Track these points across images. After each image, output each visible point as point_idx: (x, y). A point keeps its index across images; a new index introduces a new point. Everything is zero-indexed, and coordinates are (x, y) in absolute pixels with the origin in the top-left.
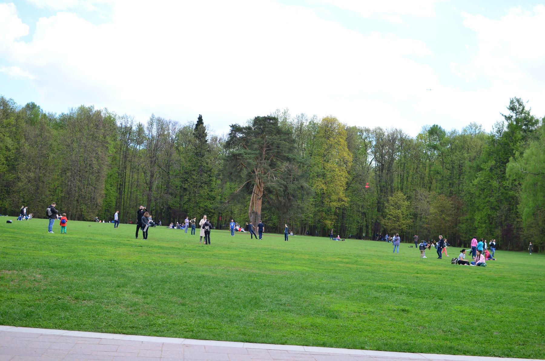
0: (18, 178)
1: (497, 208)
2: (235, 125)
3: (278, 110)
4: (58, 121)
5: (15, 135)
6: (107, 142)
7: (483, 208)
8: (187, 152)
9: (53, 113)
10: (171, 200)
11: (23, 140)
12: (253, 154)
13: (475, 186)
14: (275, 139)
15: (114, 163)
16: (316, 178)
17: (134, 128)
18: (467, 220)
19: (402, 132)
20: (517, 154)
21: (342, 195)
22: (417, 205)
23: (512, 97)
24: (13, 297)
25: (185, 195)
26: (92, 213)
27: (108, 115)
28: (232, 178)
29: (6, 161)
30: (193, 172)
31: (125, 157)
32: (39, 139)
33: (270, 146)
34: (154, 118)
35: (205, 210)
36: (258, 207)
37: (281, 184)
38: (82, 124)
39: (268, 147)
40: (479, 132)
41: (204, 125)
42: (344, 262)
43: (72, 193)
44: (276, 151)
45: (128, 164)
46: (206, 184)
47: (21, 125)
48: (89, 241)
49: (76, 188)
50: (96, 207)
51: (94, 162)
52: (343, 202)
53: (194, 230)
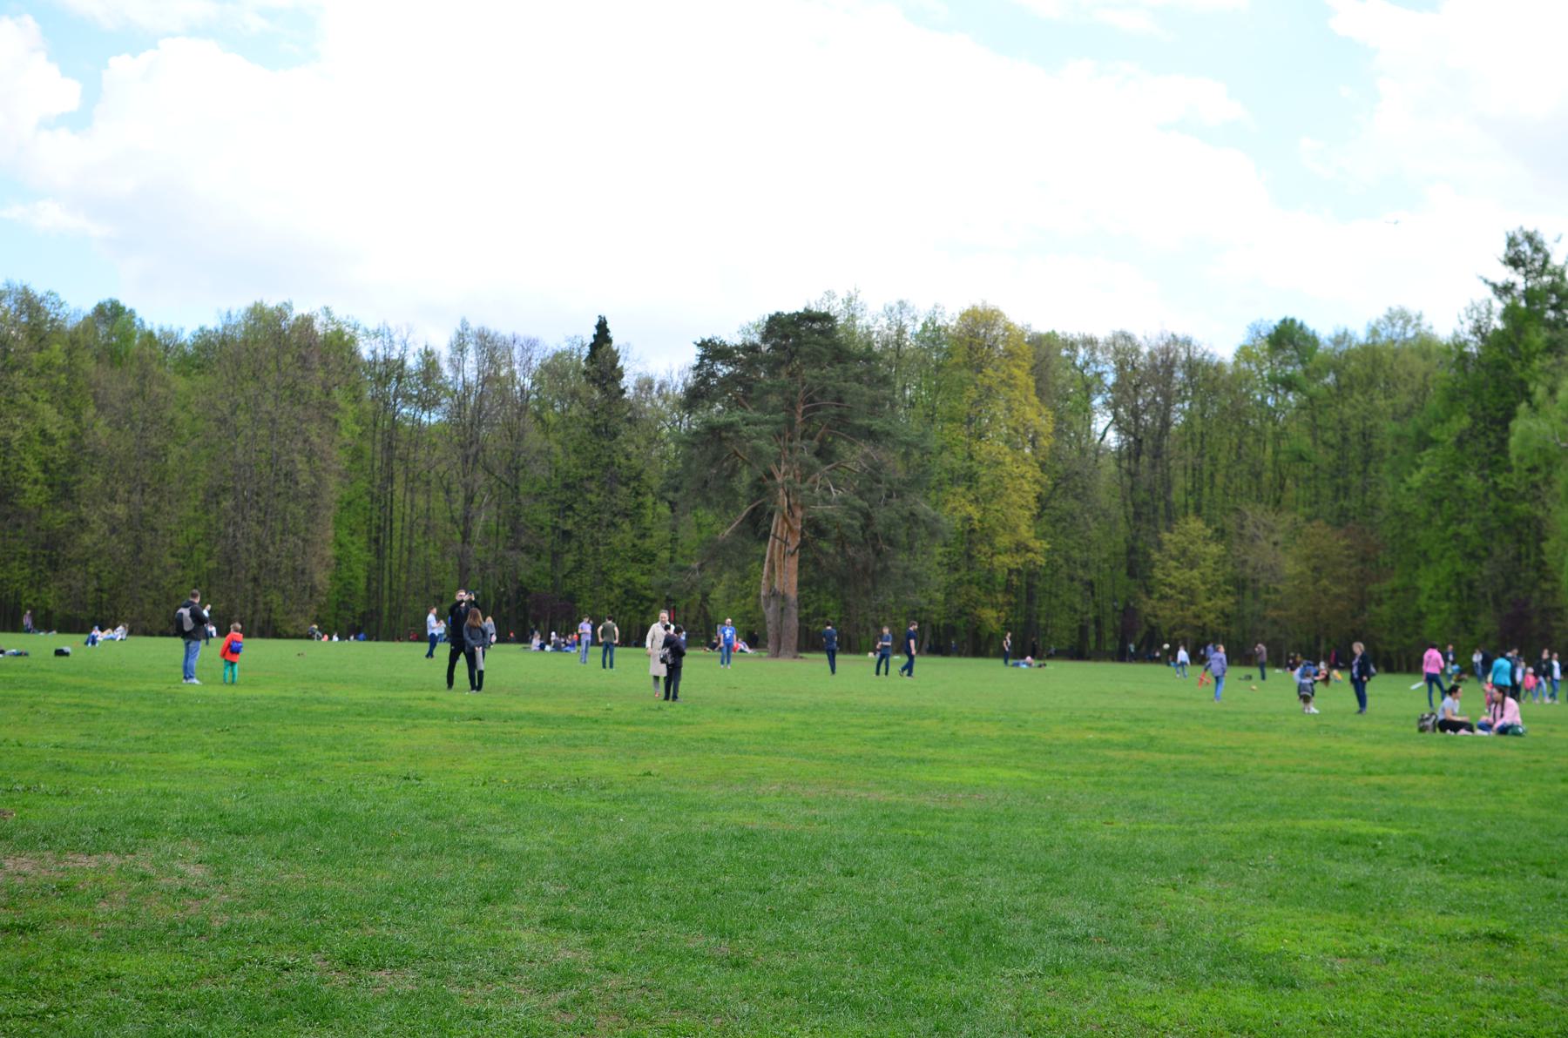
0: (82, 521)
1: (1483, 553)
2: (710, 341)
3: (831, 295)
4: (190, 350)
5: (67, 396)
6: (335, 407)
7: (1442, 556)
8: (567, 427)
9: (175, 328)
10: (527, 569)
11: (91, 411)
12: (767, 422)
13: (1414, 493)
14: (830, 378)
15: (357, 466)
16: (948, 487)
17: (412, 362)
18: (1394, 591)
19: (1194, 343)
20: (1540, 392)
21: (1025, 533)
22: (1246, 553)
23: (1513, 227)
24: (113, 970)
25: (568, 552)
26: (299, 615)
27: (334, 327)
29: (44, 472)
30: (587, 484)
31: (389, 448)
32: (137, 406)
33: (816, 398)
35: (626, 592)
36: (788, 579)
37: (854, 508)
38: (261, 356)
39: (811, 400)
40: (1417, 335)
41: (615, 345)
42: (1117, 745)
43: (238, 558)
45: (398, 467)
46: (627, 516)
47: (83, 366)
48: (314, 708)
49: (249, 542)
50: (311, 596)
52: (1030, 555)
53: (611, 654)
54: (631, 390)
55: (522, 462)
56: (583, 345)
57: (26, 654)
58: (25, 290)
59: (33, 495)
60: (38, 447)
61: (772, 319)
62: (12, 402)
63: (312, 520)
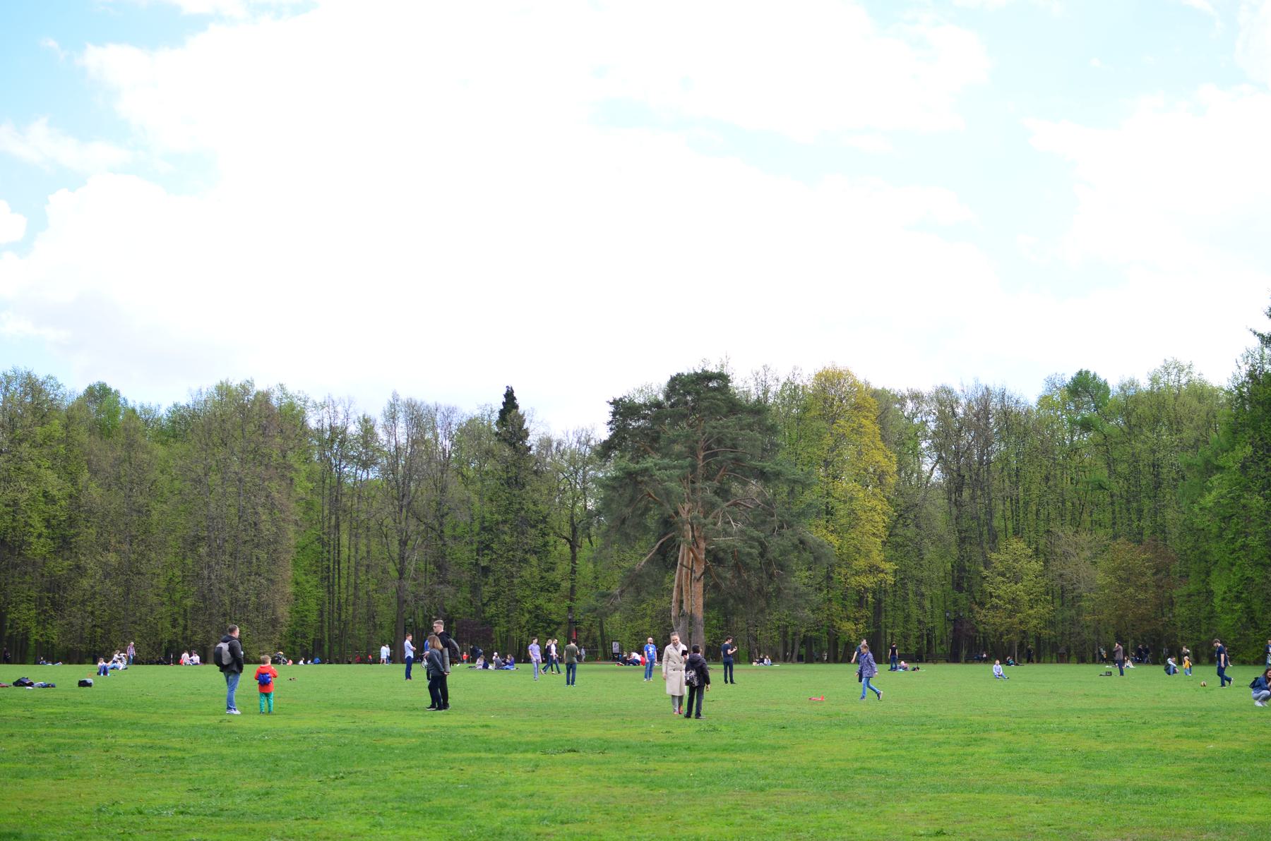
2: (621, 399)
9: (154, 405)
11: (85, 476)
12: (675, 467)
14: (728, 427)
17: (353, 429)
18: (1190, 595)
21: (877, 557)
28: (628, 531)
29: (47, 527)
34: (399, 403)
37: (752, 538)
39: (709, 448)
41: (521, 410)
44: (731, 456)
46: (536, 553)
47: (78, 438)
51: (264, 517)
52: (881, 575)
53: (574, 670)
54: (534, 448)
55: (446, 510)
56: (492, 412)
57: (53, 686)
58: (29, 376)
59: (39, 547)
60: (42, 507)
61: (673, 380)
62: (19, 469)
63: (274, 562)
